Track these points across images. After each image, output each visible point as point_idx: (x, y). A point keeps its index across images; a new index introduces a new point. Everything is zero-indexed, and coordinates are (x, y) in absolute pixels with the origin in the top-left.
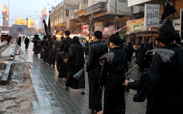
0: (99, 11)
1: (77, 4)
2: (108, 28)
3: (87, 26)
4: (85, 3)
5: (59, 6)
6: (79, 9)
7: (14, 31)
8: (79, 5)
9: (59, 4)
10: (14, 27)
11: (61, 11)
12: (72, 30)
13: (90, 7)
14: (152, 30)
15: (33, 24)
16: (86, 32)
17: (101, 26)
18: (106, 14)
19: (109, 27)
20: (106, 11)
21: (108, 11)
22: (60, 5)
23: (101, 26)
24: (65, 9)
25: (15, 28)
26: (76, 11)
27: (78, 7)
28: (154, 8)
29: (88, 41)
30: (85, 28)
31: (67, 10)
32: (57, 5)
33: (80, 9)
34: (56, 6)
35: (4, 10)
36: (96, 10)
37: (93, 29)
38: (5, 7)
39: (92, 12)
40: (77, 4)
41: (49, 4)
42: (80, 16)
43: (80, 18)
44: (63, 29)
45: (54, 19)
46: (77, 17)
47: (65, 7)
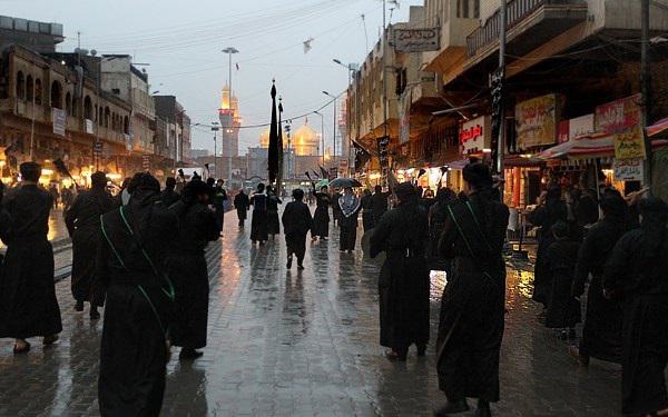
0: (538, 21)
1: (431, 27)
2: (592, 116)
3: (481, 121)
4: (466, 16)
5: (372, 59)
6: (439, 49)
7: (254, 168)
8: (440, 29)
9: (371, 54)
10: (254, 155)
11: (378, 77)
12: (426, 150)
13: (488, 21)
14: (67, 249)
15: (315, 144)
16: (476, 151)
17: (548, 114)
18: (573, 43)
19: (598, 111)
20: (582, 18)
21: (592, 19)
22: (375, 56)
23: (548, 114)
24: (393, 67)
25: (256, 160)
26: (429, 56)
27: (435, 40)
28: (270, 287)
29: (494, 156)
30: (473, 135)
31: (397, 71)
32: (364, 60)
33: (445, 44)
34: (361, 64)
35: (225, 106)
36: (523, 24)
37: (509, 131)
38: (228, 93)
39: (500, 41)
40: (432, 24)
41: (340, 60)
42: (448, 79)
43: (450, 93)
44: (385, 145)
45: (358, 112)
46: (434, 91)
47: (390, 60)
